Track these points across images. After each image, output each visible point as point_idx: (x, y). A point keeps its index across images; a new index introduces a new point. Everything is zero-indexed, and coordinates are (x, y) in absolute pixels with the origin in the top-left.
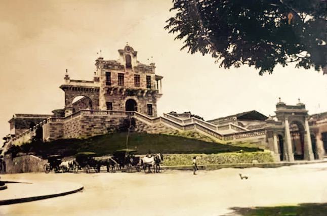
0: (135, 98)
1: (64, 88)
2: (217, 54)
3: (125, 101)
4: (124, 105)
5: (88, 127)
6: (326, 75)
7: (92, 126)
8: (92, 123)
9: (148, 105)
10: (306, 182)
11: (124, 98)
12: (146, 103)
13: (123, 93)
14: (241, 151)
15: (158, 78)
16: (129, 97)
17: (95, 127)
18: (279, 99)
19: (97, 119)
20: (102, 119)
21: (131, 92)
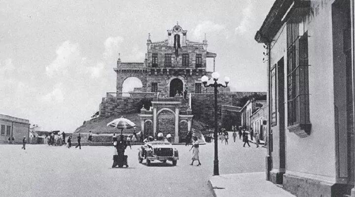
0: (181, 78)
1: (117, 71)
2: (328, 44)
3: (170, 81)
4: (169, 85)
5: (111, 108)
6: (125, 154)
7: (116, 107)
8: (116, 103)
9: (196, 84)
10: (319, 28)
11: (169, 78)
12: (194, 82)
13: (191, 74)
14: (350, 119)
15: (209, 55)
16: (173, 78)
17: (118, 107)
18: (26, 147)
19: (120, 100)
20: (125, 100)
21: (177, 73)
